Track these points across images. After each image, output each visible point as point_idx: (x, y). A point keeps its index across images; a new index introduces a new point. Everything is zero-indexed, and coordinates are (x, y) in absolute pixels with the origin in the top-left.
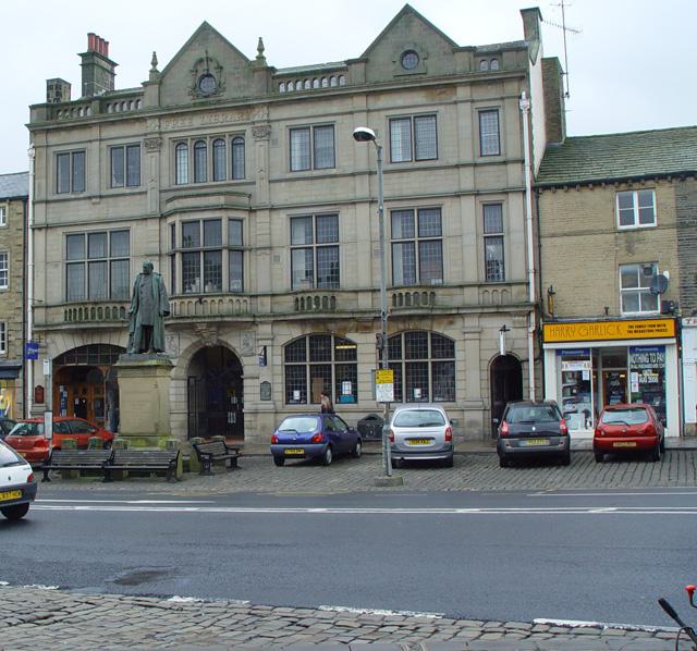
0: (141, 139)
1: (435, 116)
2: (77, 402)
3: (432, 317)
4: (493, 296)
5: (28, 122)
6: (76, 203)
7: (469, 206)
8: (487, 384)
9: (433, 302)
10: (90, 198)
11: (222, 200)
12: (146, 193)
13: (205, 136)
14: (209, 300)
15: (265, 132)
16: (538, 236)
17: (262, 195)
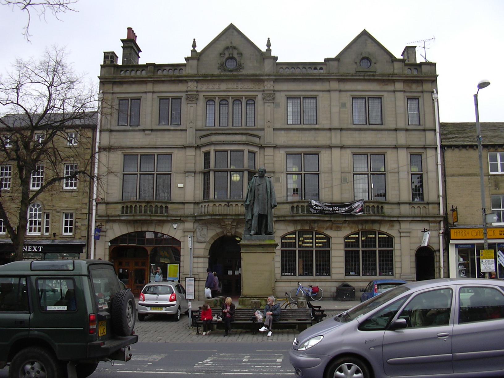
0: (184, 95)
1: (316, 98)
2: (121, 271)
3: (380, 222)
4: (419, 211)
5: (99, 75)
6: (132, 133)
7: (403, 155)
8: (414, 265)
9: (383, 212)
10: (144, 130)
11: (244, 138)
12: (185, 130)
13: (228, 97)
14: (234, 204)
15: (270, 97)
16: (444, 175)
17: (269, 137)
